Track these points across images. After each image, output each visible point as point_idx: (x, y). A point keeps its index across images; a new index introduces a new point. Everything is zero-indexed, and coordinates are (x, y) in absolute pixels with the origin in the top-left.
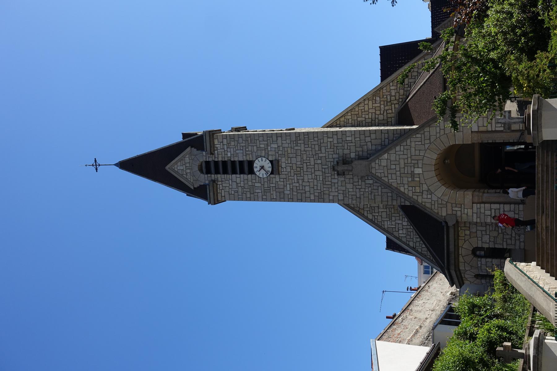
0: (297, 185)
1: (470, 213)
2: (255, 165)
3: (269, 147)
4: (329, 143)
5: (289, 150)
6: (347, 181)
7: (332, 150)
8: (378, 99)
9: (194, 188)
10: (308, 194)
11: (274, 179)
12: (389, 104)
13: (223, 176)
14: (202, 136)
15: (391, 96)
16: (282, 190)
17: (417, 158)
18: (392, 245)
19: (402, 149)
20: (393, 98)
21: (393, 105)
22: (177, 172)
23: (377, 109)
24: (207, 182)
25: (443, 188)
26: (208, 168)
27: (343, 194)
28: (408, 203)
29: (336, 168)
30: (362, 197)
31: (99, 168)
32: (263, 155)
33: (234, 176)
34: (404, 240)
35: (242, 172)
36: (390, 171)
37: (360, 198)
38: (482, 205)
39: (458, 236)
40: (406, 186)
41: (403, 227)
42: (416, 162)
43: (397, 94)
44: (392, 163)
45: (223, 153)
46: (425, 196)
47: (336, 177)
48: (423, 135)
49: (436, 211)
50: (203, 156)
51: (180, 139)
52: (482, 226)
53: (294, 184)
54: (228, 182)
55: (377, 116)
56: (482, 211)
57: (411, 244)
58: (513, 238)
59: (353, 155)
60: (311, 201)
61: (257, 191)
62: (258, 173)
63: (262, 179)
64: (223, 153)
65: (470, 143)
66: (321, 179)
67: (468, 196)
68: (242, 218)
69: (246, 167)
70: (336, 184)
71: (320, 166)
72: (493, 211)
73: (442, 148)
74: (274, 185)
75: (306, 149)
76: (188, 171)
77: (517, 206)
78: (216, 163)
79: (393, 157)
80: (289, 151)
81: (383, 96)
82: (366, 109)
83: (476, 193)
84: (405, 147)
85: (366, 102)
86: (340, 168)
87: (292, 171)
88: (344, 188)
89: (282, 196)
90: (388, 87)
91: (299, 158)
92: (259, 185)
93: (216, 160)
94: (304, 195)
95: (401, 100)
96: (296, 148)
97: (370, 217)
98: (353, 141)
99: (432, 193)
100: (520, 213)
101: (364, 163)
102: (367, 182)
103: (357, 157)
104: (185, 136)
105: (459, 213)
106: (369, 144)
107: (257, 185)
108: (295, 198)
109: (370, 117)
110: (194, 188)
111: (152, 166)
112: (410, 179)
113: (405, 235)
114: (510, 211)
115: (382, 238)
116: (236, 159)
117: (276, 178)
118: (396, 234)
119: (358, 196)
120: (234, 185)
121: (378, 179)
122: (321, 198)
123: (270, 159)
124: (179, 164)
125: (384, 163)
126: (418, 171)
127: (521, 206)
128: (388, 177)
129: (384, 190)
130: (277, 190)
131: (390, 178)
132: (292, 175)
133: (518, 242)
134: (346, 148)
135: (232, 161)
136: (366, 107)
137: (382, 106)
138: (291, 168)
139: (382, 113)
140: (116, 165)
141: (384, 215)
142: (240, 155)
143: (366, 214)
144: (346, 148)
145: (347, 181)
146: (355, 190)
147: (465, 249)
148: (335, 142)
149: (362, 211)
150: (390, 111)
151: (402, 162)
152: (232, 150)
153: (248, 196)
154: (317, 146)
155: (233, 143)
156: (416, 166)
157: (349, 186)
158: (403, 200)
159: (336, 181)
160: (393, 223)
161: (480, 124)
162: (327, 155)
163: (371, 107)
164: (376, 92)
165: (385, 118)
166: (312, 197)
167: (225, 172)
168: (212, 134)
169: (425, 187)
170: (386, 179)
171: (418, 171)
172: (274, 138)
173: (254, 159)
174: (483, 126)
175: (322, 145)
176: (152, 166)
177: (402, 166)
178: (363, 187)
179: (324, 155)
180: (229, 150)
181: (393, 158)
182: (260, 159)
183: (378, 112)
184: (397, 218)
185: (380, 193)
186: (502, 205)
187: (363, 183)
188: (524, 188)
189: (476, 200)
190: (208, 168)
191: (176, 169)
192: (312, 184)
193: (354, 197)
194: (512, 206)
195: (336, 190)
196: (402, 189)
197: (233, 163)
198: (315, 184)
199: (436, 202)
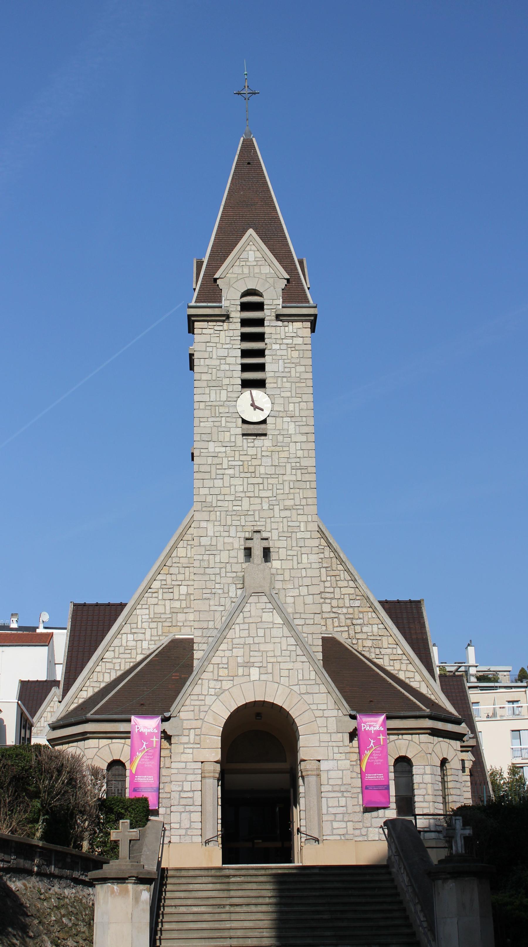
0: (225, 466)
1: (184, 757)
3: (289, 419)
4: (298, 524)
5: (286, 454)
7: (285, 530)
9: (215, 280)
11: (234, 425)
12: (349, 622)
19: (290, 648)
21: (346, 629)
24: (224, 303)
25: (226, 715)
27: (211, 545)
29: (256, 536)
30: (207, 578)
32: (276, 408)
33: (239, 353)
34: (116, 642)
37: (204, 574)
38: (199, 778)
40: (228, 653)
42: (270, 671)
43: (364, 636)
44: (268, 631)
46: (212, 684)
47: (242, 535)
48: (313, 682)
49: (187, 703)
50: (273, 301)
53: (225, 460)
55: (328, 601)
56: (190, 778)
63: (234, 403)
64: (278, 336)
66: (235, 508)
70: (226, 534)
71: (258, 507)
72: (190, 794)
73: (293, 713)
74: (223, 425)
75: (286, 484)
78: (260, 322)
80: (282, 455)
81: (362, 612)
82: (340, 584)
84: (293, 654)
85: (352, 584)
87: (249, 458)
88: (220, 547)
91: (271, 470)
92: (224, 397)
93: (266, 323)
94: (207, 476)
95: (355, 641)
96: (288, 466)
98: (300, 566)
99: (218, 696)
100: (187, 837)
102: (233, 588)
103: (274, 571)
105: (184, 739)
106: (296, 592)
107: (224, 393)
109: (327, 590)
110: (215, 280)
112: (240, 660)
113: (124, 644)
114: (191, 822)
117: (238, 429)
118: (126, 629)
119: (208, 571)
121: (239, 608)
124: (258, 254)
125: (267, 617)
126: (255, 673)
128: (244, 623)
130: (215, 430)
131: (242, 627)
132: (242, 458)
134: (290, 553)
136: (345, 584)
137: (345, 610)
138: (254, 457)
139: (334, 610)
141: (159, 609)
143: (160, 577)
144: (290, 553)
145: (233, 553)
146: (218, 565)
148: (299, 535)
149: (165, 570)
150: (336, 624)
151: (270, 647)
152: (284, 353)
154: (291, 503)
155: (295, 354)
156: (263, 670)
157: (224, 556)
159: (233, 533)
160: (145, 625)
161: (332, 774)
162: (277, 520)
163: (344, 591)
169: (226, 685)
170: (240, 620)
171: (255, 673)
173: (268, 390)
174: (329, 779)
175: (294, 512)
177: (262, 647)
178: (223, 580)
179: (277, 515)
180: (284, 347)
183: (334, 603)
184: (154, 632)
185: (213, 608)
187: (230, 580)
190: (252, 303)
191: (248, 248)
195: (217, 534)
196: (223, 647)
197: (261, 353)
198: (227, 498)
199: (202, 703)
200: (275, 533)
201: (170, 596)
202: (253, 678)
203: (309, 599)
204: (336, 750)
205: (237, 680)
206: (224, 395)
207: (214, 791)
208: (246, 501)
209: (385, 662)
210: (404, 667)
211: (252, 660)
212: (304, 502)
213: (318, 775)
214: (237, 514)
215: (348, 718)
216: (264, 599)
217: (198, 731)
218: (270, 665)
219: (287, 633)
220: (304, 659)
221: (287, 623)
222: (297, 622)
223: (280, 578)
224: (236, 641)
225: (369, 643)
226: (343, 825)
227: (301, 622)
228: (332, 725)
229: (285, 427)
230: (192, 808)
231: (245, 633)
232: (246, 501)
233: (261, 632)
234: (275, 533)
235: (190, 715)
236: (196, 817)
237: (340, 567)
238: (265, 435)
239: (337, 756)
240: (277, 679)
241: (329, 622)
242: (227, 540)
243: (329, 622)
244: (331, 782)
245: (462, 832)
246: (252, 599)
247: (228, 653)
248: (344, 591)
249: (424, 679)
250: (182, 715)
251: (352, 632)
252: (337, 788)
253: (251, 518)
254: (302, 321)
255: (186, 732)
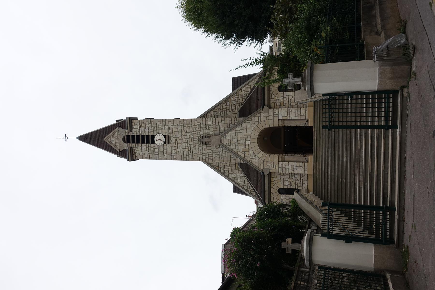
0: (179, 150)
2: (155, 138)
5: (175, 129)
6: (208, 148)
8: (228, 103)
9: (120, 151)
10: (185, 156)
13: (136, 144)
14: (125, 121)
15: (235, 101)
16: (170, 153)
17: (247, 134)
18: (236, 190)
20: (236, 103)
22: (110, 142)
23: (227, 108)
24: (127, 148)
25: (262, 152)
26: (127, 139)
28: (242, 162)
29: (201, 140)
30: (216, 157)
31: (67, 140)
32: (160, 132)
33: (143, 144)
34: (241, 185)
35: (148, 142)
36: (232, 142)
37: (215, 158)
38: (284, 163)
39: (270, 181)
40: (241, 151)
41: (241, 176)
43: (239, 100)
44: (233, 137)
45: (138, 131)
46: (251, 157)
50: (126, 133)
51: (115, 122)
52: (283, 175)
53: (177, 150)
54: (139, 148)
57: (245, 188)
58: (301, 183)
59: (211, 133)
60: (187, 160)
61: (156, 153)
62: (156, 143)
65: (277, 126)
67: (275, 157)
68: (148, 170)
69: (150, 140)
72: (290, 166)
73: (262, 129)
76: (117, 141)
77: (303, 163)
78: (133, 137)
79: (234, 134)
80: (175, 130)
82: (221, 108)
83: (281, 156)
85: (221, 105)
86: (204, 140)
87: (176, 142)
88: (206, 152)
89: (170, 157)
90: (234, 96)
91: (180, 134)
92: (157, 150)
93: (133, 135)
94: (183, 156)
96: (179, 128)
97: (222, 171)
98: (212, 125)
101: (218, 137)
102: (219, 149)
103: (214, 134)
104: (117, 121)
106: (221, 126)
107: (156, 150)
108: (178, 158)
110: (120, 151)
111: (97, 139)
112: (243, 147)
115: (230, 186)
116: (144, 134)
119: (214, 157)
120: (143, 150)
121: (225, 147)
122: (192, 158)
123: (164, 135)
124: (112, 137)
125: (228, 137)
126: (248, 142)
127: (306, 163)
129: (229, 154)
130: (168, 153)
132: (177, 144)
133: (304, 185)
134: (207, 128)
135: (142, 136)
136: (221, 107)
137: (230, 107)
138: (176, 140)
140: (77, 138)
141: (230, 170)
142: (147, 132)
143: (220, 169)
144: (207, 128)
147: (275, 189)
148: (202, 125)
150: (235, 110)
151: (239, 136)
153: (151, 156)
154: (191, 127)
155: (143, 125)
156: (247, 139)
157: (209, 151)
158: (239, 160)
159: (201, 148)
160: (235, 175)
163: (224, 107)
164: (228, 98)
165: (232, 114)
166: (187, 157)
167: (138, 142)
168: (132, 120)
169: (252, 152)
170: (230, 147)
171: (248, 142)
172: (167, 122)
176: (97, 139)
178: (217, 152)
179: (195, 133)
181: (234, 135)
182: (158, 135)
183: (228, 111)
184: (237, 172)
185: (226, 156)
186: (295, 163)
188: (266, 46)
189: (280, 160)
192: (187, 150)
193: (212, 158)
194: (301, 163)
196: (239, 153)
197: (143, 137)
198: (190, 150)
200: (201, 133)
201: (226, 166)
202: (249, 143)
203: (223, 122)
204: (275, 114)
205: (250, 148)
206: (156, 150)
207: (288, 157)
208: (190, 143)
209: (248, 93)
210: (249, 87)
211: (243, 143)
212: (191, 123)
213: (284, 120)
214: (195, 146)
215: (264, 109)
216: (222, 138)
217: (268, 163)
218: (245, 137)
219: (234, 131)
220: (243, 125)
221: (230, 130)
222: (231, 126)
223: (216, 132)
224: (237, 149)
225: (241, 99)
226: (302, 111)
227: (231, 124)
228: (266, 115)
229: (166, 129)
230: (295, 166)
231: (234, 145)
232: (190, 143)
233: (234, 140)
234: (201, 133)
235: (262, 165)
236: (298, 164)
237: (216, 109)
238: (169, 136)
239: (277, 113)
240: (250, 134)
241: (234, 112)
242: (203, 150)
243: (234, 112)
244: (286, 115)
245: (290, 79)
246: (223, 142)
247: (241, 151)
248: (224, 107)
249: (254, 80)
250: (262, 168)
251: (238, 105)
252: (289, 113)
253: (196, 142)
254: (132, 123)
255: (268, 167)
